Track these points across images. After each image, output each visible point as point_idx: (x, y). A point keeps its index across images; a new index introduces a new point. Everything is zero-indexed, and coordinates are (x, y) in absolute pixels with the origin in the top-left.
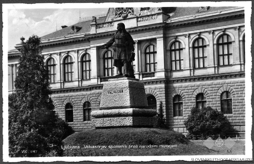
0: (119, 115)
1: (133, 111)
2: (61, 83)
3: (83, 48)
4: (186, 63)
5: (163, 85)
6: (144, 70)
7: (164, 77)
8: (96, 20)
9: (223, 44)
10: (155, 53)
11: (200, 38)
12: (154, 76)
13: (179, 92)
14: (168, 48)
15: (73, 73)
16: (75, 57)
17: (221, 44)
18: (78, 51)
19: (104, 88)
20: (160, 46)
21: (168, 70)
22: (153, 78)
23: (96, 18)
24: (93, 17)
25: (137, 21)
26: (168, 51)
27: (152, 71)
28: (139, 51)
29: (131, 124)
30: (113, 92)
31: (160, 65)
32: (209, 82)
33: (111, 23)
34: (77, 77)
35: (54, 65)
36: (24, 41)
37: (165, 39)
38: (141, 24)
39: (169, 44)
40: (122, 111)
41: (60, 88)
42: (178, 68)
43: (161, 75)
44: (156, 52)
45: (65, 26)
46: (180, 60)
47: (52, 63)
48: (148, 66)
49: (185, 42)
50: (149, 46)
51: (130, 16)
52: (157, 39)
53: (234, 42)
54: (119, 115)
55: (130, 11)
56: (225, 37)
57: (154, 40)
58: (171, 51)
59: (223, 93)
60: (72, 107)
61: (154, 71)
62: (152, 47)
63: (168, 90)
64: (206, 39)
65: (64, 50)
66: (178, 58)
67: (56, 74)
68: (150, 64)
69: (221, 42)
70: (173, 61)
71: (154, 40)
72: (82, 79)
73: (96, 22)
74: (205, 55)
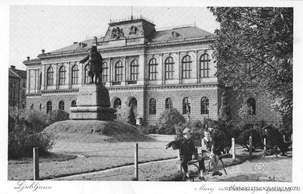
0: (88, 111)
1: (98, 108)
2: (179, 79)
3: (185, 50)
4: (159, 76)
5: (142, 90)
6: (114, 79)
7: (143, 84)
8: (97, 39)
9: (204, 61)
10: (138, 66)
11: (205, 54)
12: (136, 83)
13: (153, 96)
14: (148, 63)
15: (209, 70)
16: (176, 58)
17: (151, 65)
18: (45, 65)
19: (79, 91)
20: (141, 61)
21: (147, 80)
22: (135, 85)
23: (96, 38)
24: (95, 37)
25: (126, 42)
26: (149, 65)
27: (136, 79)
28: (127, 64)
29: (96, 118)
30: (85, 94)
31: (141, 75)
32: (66, 94)
33: (107, 42)
34: (81, 81)
35: (65, 71)
36: (96, 45)
37: (146, 56)
38: (128, 44)
39: (148, 61)
40: (90, 108)
41: (68, 88)
42: (188, 76)
43: (141, 83)
44: (138, 66)
45: (76, 43)
46: (77, 78)
47: (171, 62)
48: (133, 75)
49: (160, 60)
50: (134, 61)
51: (121, 38)
52: (140, 56)
53: (193, 61)
54: (88, 111)
55: (121, 34)
56: (171, 59)
57: (138, 56)
58: (150, 65)
59: (184, 98)
60: (63, 104)
61: (137, 79)
62: (136, 61)
63: (146, 94)
64: (174, 58)
65: (184, 49)
66: (206, 67)
67: (157, 72)
68: (50, 79)
69: (202, 59)
70: (151, 73)
71: (138, 56)
72: (59, 84)
73: (96, 40)
74: (190, 69)
